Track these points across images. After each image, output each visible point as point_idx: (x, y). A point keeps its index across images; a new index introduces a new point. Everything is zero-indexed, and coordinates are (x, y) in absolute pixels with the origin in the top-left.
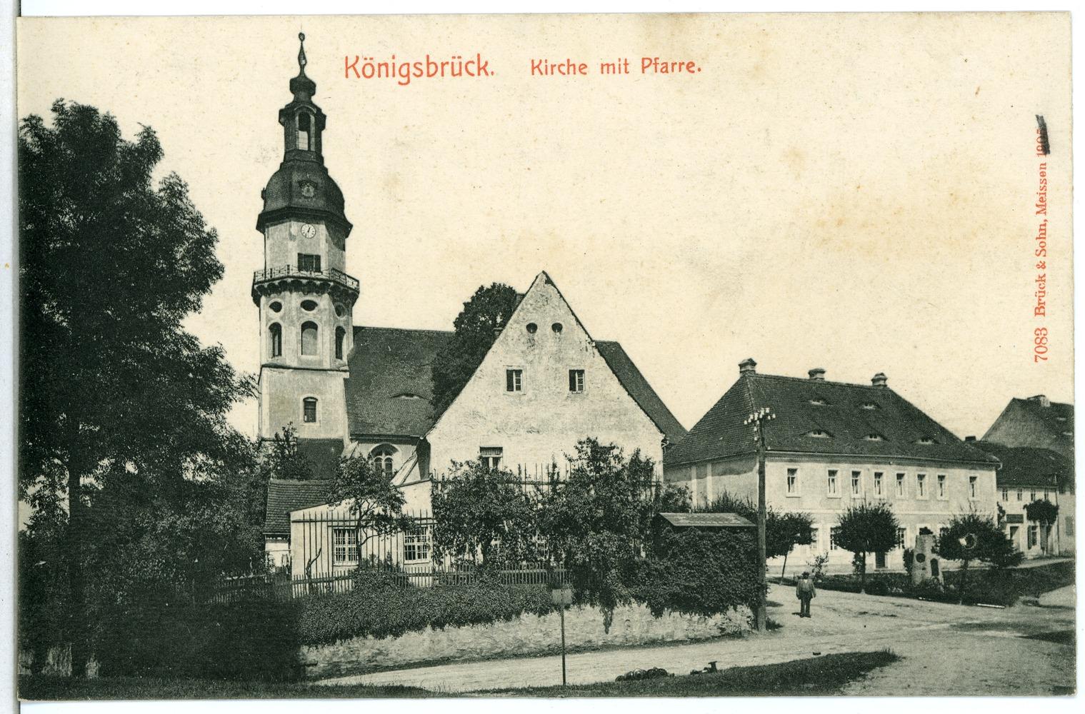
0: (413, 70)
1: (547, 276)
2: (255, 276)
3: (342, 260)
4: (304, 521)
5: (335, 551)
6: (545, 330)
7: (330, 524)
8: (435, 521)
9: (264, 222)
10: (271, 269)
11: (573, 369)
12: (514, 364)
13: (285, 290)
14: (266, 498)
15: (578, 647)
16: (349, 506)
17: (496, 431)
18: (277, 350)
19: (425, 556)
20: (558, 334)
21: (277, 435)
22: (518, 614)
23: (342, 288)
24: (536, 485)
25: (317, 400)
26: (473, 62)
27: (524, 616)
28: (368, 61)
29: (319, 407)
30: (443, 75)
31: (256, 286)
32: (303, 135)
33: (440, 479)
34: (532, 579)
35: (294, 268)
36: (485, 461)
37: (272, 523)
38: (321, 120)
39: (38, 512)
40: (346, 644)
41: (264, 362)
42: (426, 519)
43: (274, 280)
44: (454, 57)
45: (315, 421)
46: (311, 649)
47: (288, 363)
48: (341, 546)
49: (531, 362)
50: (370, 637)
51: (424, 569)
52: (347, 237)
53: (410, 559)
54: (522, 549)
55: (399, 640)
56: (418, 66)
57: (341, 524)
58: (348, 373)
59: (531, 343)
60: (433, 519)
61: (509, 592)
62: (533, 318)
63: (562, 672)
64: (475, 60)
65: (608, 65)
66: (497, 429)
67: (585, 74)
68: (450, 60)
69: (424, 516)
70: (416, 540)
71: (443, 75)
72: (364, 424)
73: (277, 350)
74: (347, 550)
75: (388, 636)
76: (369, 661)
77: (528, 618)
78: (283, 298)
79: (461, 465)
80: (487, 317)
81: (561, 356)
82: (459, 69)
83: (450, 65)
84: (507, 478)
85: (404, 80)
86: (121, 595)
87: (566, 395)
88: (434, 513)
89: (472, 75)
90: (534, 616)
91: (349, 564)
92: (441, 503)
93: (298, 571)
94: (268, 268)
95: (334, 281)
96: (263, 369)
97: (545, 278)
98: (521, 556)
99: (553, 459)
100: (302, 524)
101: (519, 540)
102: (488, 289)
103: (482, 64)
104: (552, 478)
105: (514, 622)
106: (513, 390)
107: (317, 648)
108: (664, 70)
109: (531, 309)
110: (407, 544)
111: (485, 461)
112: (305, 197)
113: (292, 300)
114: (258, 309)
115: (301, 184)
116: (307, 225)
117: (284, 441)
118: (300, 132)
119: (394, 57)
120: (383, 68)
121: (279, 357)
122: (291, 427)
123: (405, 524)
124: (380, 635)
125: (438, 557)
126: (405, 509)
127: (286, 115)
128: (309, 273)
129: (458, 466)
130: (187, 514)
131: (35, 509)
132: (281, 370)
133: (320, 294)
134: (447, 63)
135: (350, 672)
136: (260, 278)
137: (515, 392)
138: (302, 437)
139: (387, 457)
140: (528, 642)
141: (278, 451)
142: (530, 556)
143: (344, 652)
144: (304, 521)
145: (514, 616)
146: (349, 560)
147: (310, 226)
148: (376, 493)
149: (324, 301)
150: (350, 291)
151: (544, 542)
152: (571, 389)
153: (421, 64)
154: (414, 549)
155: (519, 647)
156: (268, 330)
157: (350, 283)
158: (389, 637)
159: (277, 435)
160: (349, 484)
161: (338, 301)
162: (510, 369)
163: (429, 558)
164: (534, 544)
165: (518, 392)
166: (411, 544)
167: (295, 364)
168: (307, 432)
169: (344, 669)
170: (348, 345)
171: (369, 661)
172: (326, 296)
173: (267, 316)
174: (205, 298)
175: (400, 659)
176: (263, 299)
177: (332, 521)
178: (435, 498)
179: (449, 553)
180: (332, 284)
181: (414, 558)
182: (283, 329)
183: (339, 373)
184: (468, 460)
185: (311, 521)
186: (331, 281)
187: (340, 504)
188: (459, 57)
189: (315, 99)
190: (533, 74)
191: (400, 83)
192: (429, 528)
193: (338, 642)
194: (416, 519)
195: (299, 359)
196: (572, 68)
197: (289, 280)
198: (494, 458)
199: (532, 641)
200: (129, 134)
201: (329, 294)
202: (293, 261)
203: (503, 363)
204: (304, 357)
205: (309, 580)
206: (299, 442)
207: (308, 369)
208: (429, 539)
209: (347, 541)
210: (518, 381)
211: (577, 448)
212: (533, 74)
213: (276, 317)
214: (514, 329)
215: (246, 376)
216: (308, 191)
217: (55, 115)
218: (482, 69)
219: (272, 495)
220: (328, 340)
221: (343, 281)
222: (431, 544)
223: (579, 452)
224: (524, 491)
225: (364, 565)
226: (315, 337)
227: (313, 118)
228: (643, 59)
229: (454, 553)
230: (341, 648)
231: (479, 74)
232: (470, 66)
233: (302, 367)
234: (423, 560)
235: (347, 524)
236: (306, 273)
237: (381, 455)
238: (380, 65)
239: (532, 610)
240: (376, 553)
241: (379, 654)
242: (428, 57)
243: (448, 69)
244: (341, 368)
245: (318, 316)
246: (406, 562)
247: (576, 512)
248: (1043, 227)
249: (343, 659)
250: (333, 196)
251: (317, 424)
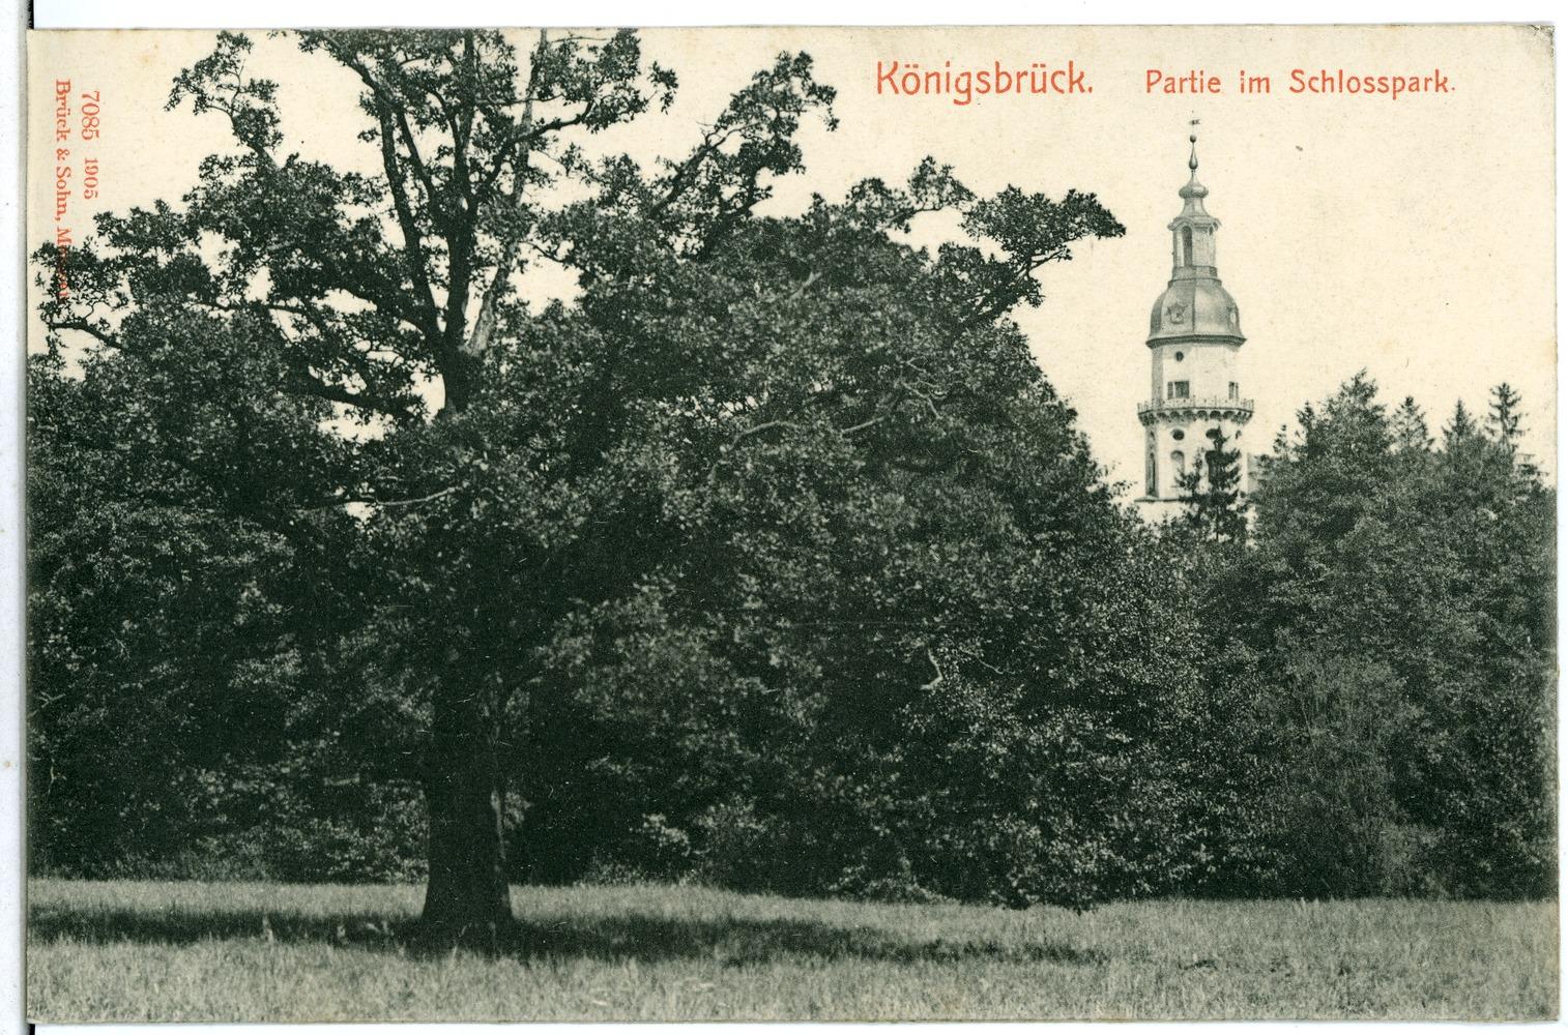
0: (975, 83)
26: (1063, 73)
28: (911, 70)
30: (1019, 90)
44: (1035, 66)
56: (983, 77)
64: (1066, 69)
65: (1259, 80)
67: (175, 100)
68: (1030, 70)
71: (1019, 90)
82: (1043, 82)
83: (1029, 77)
85: (963, 98)
89: (1062, 91)
103: (1076, 76)
108: (1169, 88)
119: (948, 64)
120: (933, 80)
134: (1026, 73)
153: (988, 74)
188: (1043, 66)
190: (880, 91)
191: (956, 102)
196: (1328, 84)
212: (880, 91)
218: (1076, 82)
228: (1149, 72)
231: (1071, 90)
232: (1057, 79)
238: (928, 76)
242: (997, 64)
243: (1026, 81)
248: (62, 209)
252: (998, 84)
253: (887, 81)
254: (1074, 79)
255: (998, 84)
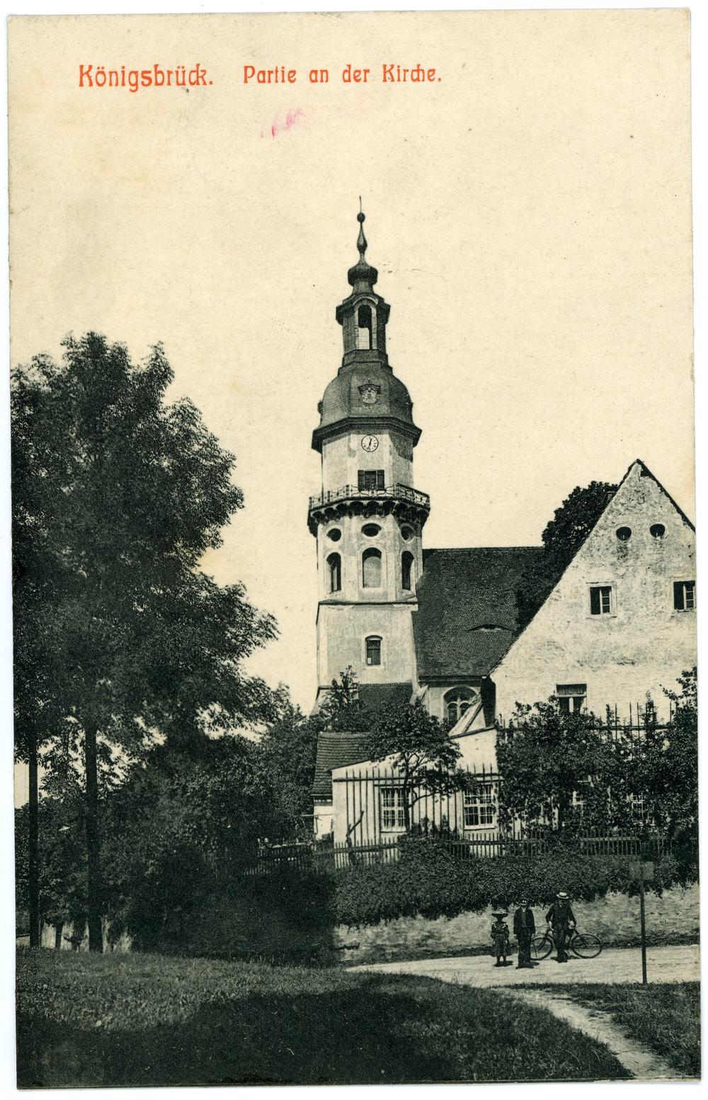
1: (644, 467)
2: (311, 502)
3: (409, 475)
4: (347, 780)
5: (383, 815)
6: (641, 534)
7: (376, 782)
8: (501, 778)
9: (318, 441)
10: (329, 492)
11: (678, 580)
12: (600, 581)
13: (344, 515)
14: (315, 754)
15: (682, 936)
16: (393, 761)
17: (578, 665)
18: (336, 585)
19: (490, 821)
20: (658, 538)
21: (334, 682)
22: (602, 892)
23: (409, 506)
24: (627, 730)
25: (381, 638)
27: (610, 895)
28: (101, 70)
29: (384, 647)
31: (312, 513)
32: (364, 333)
33: (507, 727)
34: (621, 848)
35: (353, 489)
36: (564, 702)
37: (321, 783)
38: (384, 310)
39: (50, 773)
40: (390, 925)
41: (322, 599)
42: (491, 775)
43: (333, 503)
44: (179, 67)
45: (379, 664)
46: (352, 929)
47: (348, 599)
48: (390, 809)
49: (623, 576)
50: (419, 916)
51: (488, 836)
52: (415, 444)
53: (472, 824)
54: (612, 810)
55: (455, 921)
57: (389, 782)
58: (417, 606)
59: (623, 553)
60: (498, 775)
61: (590, 865)
62: (622, 522)
63: (641, 969)
66: (578, 662)
69: (488, 771)
70: (478, 801)
72: (436, 664)
73: (336, 585)
74: (396, 813)
75: (441, 916)
76: (419, 945)
77: (615, 898)
78: (343, 524)
79: (529, 708)
80: (586, 525)
81: (663, 566)
84: (589, 723)
85: (134, 88)
86: (152, 864)
87: (670, 615)
88: (500, 768)
90: (624, 896)
91: (399, 830)
92: (509, 756)
93: (340, 839)
94: (325, 491)
95: (400, 499)
96: (321, 606)
97: (640, 468)
98: (611, 820)
99: (648, 695)
100: (345, 783)
101: (609, 800)
102: (584, 490)
104: (646, 720)
105: (598, 903)
106: (599, 613)
107: (358, 928)
109: (622, 510)
110: (465, 806)
111: (564, 702)
112: (366, 404)
113: (352, 525)
114: (315, 539)
115: (361, 389)
116: (368, 437)
117: (341, 688)
118: (360, 329)
121: (338, 592)
122: (350, 672)
123: (464, 782)
124: (430, 914)
125: (505, 820)
126: (462, 764)
127: (343, 313)
128: (370, 492)
129: (525, 710)
130: (218, 774)
131: (48, 771)
132: (340, 606)
133: (383, 516)
135: (396, 958)
136: (317, 504)
137: (603, 615)
138: (364, 682)
139: (463, 702)
140: (615, 928)
141: (336, 700)
142: (622, 820)
143: (389, 933)
144: (347, 780)
145: (597, 896)
146: (399, 825)
147: (372, 437)
148: (424, 744)
149: (388, 525)
150: (419, 509)
151: (641, 802)
152: (676, 607)
154: (476, 811)
155: (604, 934)
156: (326, 562)
157: (418, 499)
158: (442, 918)
159: (334, 682)
160: (394, 735)
161: (405, 522)
162: (595, 586)
163: (495, 823)
164: (628, 805)
165: (607, 615)
166: (473, 805)
167: (356, 599)
168: (370, 676)
169: (389, 954)
170: (417, 572)
171: (419, 945)
172: (390, 517)
173: (325, 547)
174: (224, 531)
175: (454, 943)
176: (320, 527)
177: (379, 779)
178: (500, 750)
179: (520, 816)
180: (397, 502)
181: (477, 823)
182: (342, 560)
183: (407, 606)
184: (537, 701)
185: (354, 780)
186: (396, 499)
187: (384, 760)
188: (183, 67)
189: (377, 289)
192: (494, 787)
193: (383, 921)
194: (479, 775)
195: (360, 593)
197: (349, 503)
198: (574, 698)
199: (621, 927)
200: (139, 360)
201: (394, 514)
202: (353, 481)
203: (584, 581)
204: (366, 590)
205: (352, 851)
206: (366, 690)
207: (369, 604)
208: (494, 800)
209: (396, 803)
210: (606, 601)
211: (680, 681)
213: (334, 547)
214: (602, 535)
215: (266, 615)
216: (369, 396)
217: (64, 349)
219: (322, 752)
220: (393, 569)
221: (409, 498)
222: (496, 805)
223: (684, 687)
224: (614, 738)
225: (414, 831)
226: (379, 567)
227: (374, 311)
229: (525, 816)
230: (385, 929)
233: (364, 601)
234: (487, 826)
235: (396, 782)
236: (367, 492)
237: (456, 701)
239: (620, 888)
240: (430, 817)
241: (429, 937)
244: (409, 600)
245: (381, 541)
246: (467, 827)
247: (677, 764)
249: (387, 943)
250: (400, 398)
251: (381, 667)
252: (137, 77)
253: (85, 75)
254: (84, 72)
255: (137, 77)
